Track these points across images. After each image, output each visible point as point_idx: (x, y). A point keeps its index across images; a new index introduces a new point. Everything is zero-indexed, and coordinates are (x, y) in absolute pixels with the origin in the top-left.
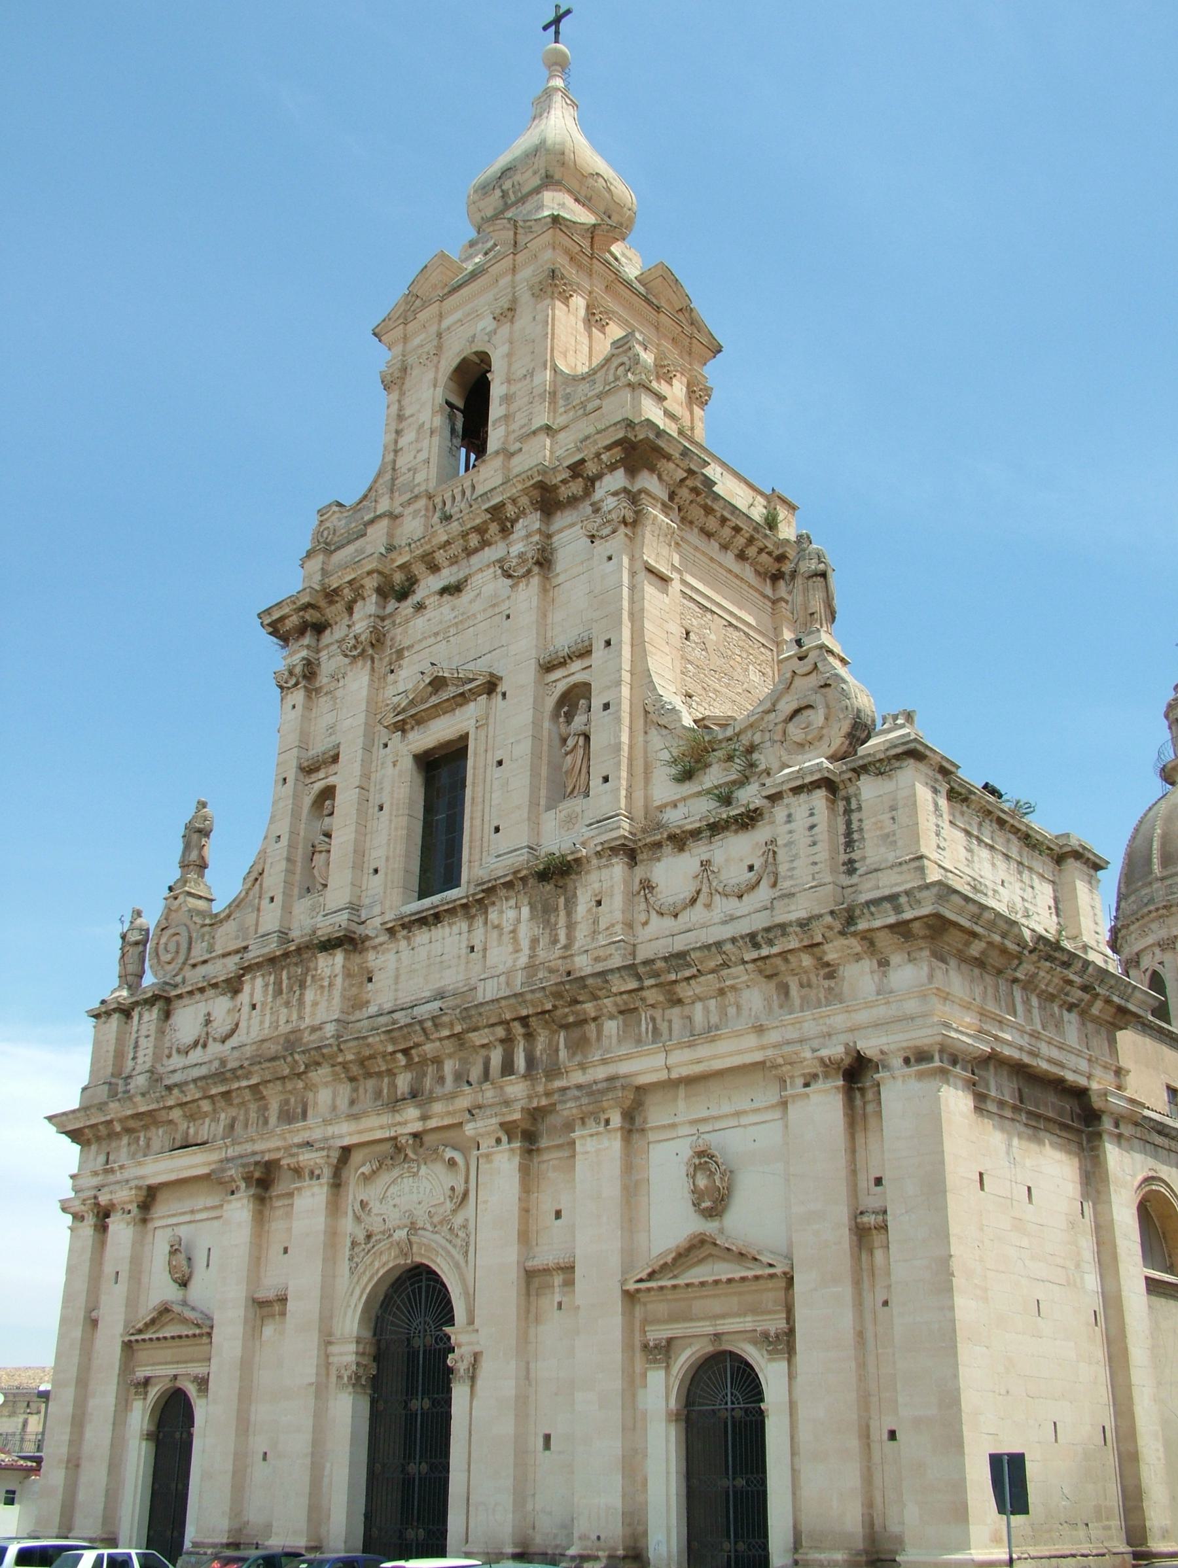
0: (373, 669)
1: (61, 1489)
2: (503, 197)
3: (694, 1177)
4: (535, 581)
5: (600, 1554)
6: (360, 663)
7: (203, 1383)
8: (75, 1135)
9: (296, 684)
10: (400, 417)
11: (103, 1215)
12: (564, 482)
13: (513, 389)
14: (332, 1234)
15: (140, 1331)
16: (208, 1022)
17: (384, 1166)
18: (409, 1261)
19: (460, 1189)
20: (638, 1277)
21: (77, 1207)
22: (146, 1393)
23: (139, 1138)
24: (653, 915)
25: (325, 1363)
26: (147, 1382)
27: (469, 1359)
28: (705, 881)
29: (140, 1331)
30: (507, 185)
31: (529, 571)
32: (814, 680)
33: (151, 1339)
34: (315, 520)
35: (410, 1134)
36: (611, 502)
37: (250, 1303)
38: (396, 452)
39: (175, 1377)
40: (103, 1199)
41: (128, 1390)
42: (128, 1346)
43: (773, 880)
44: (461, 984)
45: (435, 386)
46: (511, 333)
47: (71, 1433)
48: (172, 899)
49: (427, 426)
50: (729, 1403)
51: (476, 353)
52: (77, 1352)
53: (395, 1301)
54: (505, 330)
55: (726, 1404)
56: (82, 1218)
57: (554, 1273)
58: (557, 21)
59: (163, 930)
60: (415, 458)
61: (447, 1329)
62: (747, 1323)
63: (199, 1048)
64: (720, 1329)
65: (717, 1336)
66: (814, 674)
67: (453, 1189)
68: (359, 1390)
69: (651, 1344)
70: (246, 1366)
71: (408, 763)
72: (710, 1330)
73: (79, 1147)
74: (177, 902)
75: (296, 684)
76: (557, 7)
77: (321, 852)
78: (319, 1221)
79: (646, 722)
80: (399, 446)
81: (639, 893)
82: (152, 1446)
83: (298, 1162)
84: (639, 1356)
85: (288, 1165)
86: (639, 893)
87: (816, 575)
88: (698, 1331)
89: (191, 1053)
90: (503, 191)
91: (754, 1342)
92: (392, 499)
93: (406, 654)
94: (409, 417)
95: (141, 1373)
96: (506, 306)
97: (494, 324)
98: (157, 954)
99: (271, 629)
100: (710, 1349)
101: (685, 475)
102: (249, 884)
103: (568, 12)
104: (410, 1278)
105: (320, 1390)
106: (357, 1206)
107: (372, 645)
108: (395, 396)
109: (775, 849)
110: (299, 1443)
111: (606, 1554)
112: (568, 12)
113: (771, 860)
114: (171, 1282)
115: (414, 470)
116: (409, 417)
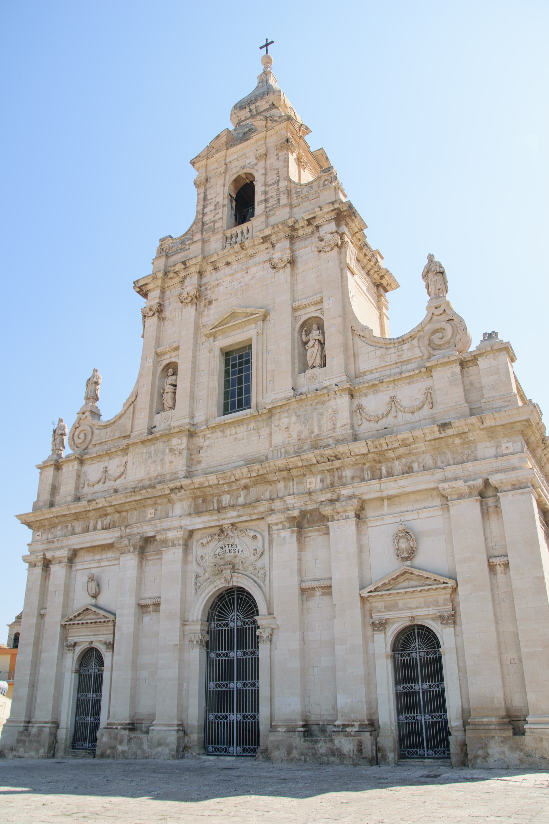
0: (196, 309)
1: (26, 697)
2: (250, 112)
3: (398, 542)
4: (288, 269)
5: (355, 723)
6: (190, 306)
7: (111, 646)
8: (29, 525)
9: (153, 315)
10: (205, 199)
11: (47, 564)
12: (302, 227)
13: (267, 189)
14: (184, 572)
15: (71, 620)
16: (106, 471)
17: (214, 540)
18: (231, 585)
19: (260, 551)
20: (369, 590)
21: (33, 558)
22: (74, 650)
23: (67, 526)
24: (364, 420)
25: (183, 635)
26: (75, 644)
27: (268, 631)
28: (393, 405)
29: (71, 620)
30: (253, 107)
31: (285, 266)
32: (444, 317)
33: (78, 624)
34: (158, 244)
35: (230, 524)
36: (329, 236)
37: (137, 605)
38: (204, 214)
39: (92, 642)
40: (49, 555)
41: (63, 649)
42: (64, 627)
43: (431, 405)
44: (255, 453)
45: (224, 186)
46: (265, 165)
47: (31, 670)
48: (81, 414)
49: (221, 203)
50: (417, 649)
51: (245, 174)
52: (34, 630)
53: (219, 605)
54: (262, 163)
55: (416, 650)
56: (35, 565)
57: (317, 589)
58: (267, 45)
59: (76, 428)
60: (214, 216)
61: (256, 617)
62: (431, 611)
63: (101, 483)
64: (414, 614)
65: (413, 618)
66: (444, 314)
67: (256, 550)
68: (202, 647)
69: (377, 622)
70: (137, 636)
71: (218, 353)
72: (410, 615)
73: (32, 531)
74: (84, 416)
75: (153, 315)
76: (267, 40)
77: (167, 392)
78: (178, 566)
79: (352, 335)
80: (205, 212)
81: (356, 411)
82: (77, 675)
83: (166, 538)
84: (369, 629)
85: (160, 539)
86: (356, 411)
87: (439, 272)
88: (403, 615)
89: (96, 486)
90: (250, 109)
91: (433, 619)
92: (202, 234)
93: (214, 302)
94: (210, 199)
95: (71, 640)
96: (264, 153)
97: (256, 161)
98: (73, 439)
99: (139, 290)
100: (409, 623)
101: (358, 230)
102: (126, 407)
103: (272, 42)
104: (227, 594)
105: (181, 648)
106: (199, 559)
107: (196, 297)
108: (202, 190)
109: (431, 392)
110: (172, 673)
111: (359, 723)
112: (272, 42)
113: (429, 396)
114: (88, 596)
115: (214, 222)
116: (210, 199)
